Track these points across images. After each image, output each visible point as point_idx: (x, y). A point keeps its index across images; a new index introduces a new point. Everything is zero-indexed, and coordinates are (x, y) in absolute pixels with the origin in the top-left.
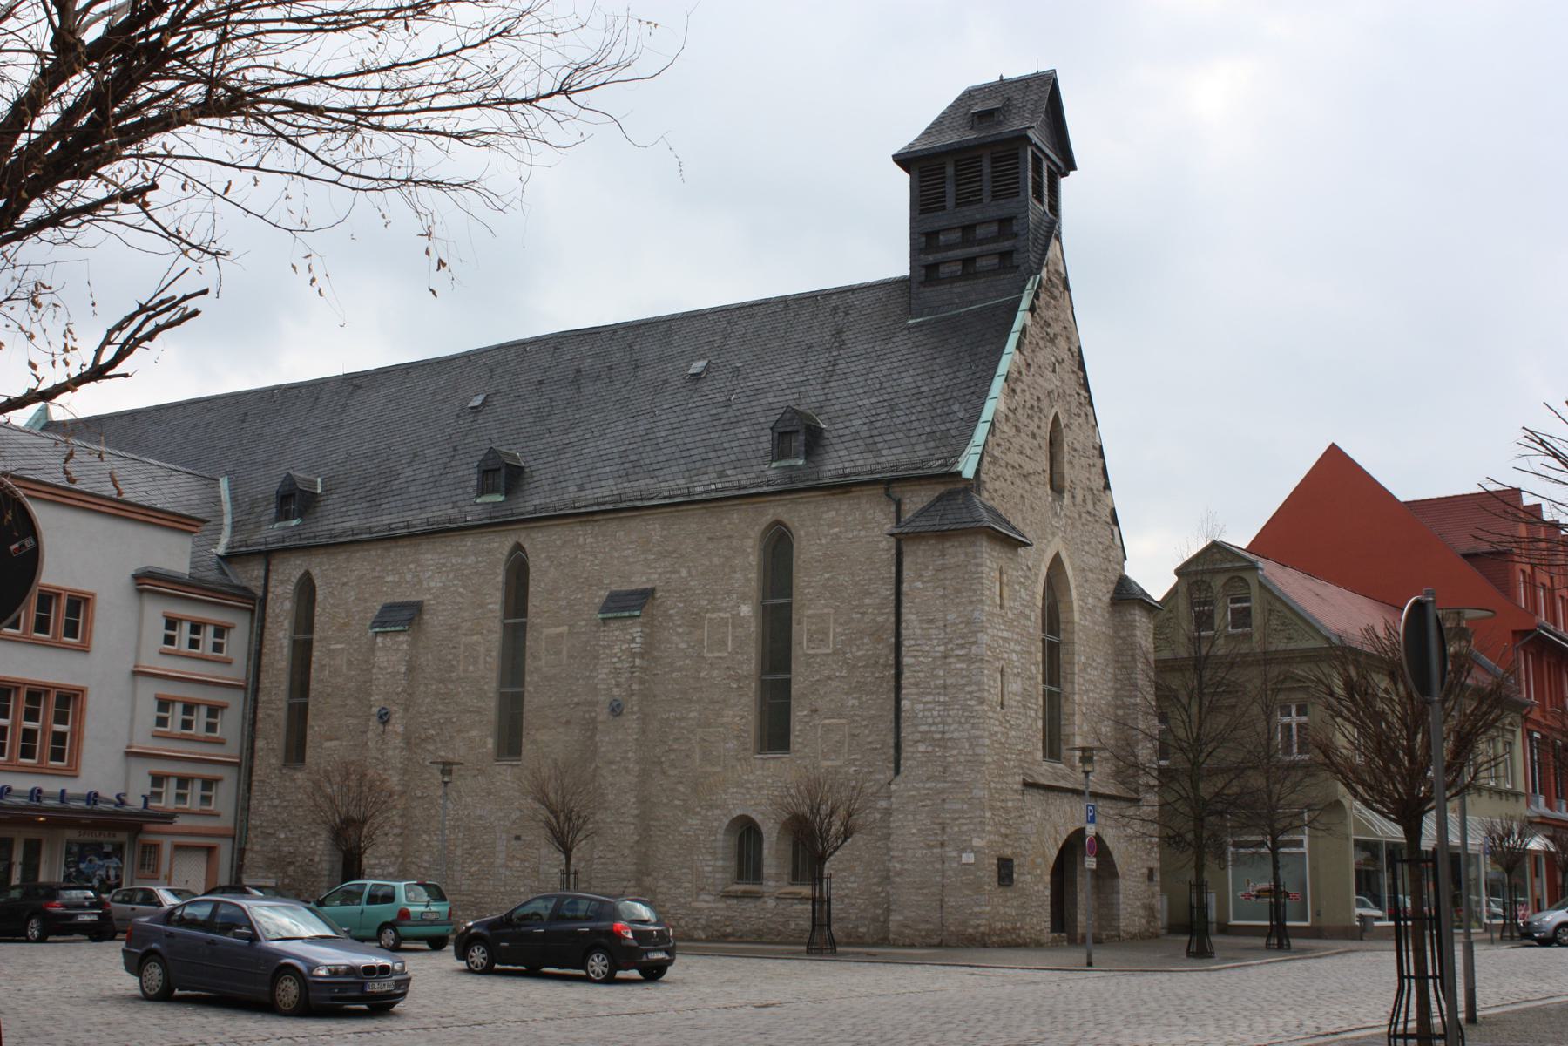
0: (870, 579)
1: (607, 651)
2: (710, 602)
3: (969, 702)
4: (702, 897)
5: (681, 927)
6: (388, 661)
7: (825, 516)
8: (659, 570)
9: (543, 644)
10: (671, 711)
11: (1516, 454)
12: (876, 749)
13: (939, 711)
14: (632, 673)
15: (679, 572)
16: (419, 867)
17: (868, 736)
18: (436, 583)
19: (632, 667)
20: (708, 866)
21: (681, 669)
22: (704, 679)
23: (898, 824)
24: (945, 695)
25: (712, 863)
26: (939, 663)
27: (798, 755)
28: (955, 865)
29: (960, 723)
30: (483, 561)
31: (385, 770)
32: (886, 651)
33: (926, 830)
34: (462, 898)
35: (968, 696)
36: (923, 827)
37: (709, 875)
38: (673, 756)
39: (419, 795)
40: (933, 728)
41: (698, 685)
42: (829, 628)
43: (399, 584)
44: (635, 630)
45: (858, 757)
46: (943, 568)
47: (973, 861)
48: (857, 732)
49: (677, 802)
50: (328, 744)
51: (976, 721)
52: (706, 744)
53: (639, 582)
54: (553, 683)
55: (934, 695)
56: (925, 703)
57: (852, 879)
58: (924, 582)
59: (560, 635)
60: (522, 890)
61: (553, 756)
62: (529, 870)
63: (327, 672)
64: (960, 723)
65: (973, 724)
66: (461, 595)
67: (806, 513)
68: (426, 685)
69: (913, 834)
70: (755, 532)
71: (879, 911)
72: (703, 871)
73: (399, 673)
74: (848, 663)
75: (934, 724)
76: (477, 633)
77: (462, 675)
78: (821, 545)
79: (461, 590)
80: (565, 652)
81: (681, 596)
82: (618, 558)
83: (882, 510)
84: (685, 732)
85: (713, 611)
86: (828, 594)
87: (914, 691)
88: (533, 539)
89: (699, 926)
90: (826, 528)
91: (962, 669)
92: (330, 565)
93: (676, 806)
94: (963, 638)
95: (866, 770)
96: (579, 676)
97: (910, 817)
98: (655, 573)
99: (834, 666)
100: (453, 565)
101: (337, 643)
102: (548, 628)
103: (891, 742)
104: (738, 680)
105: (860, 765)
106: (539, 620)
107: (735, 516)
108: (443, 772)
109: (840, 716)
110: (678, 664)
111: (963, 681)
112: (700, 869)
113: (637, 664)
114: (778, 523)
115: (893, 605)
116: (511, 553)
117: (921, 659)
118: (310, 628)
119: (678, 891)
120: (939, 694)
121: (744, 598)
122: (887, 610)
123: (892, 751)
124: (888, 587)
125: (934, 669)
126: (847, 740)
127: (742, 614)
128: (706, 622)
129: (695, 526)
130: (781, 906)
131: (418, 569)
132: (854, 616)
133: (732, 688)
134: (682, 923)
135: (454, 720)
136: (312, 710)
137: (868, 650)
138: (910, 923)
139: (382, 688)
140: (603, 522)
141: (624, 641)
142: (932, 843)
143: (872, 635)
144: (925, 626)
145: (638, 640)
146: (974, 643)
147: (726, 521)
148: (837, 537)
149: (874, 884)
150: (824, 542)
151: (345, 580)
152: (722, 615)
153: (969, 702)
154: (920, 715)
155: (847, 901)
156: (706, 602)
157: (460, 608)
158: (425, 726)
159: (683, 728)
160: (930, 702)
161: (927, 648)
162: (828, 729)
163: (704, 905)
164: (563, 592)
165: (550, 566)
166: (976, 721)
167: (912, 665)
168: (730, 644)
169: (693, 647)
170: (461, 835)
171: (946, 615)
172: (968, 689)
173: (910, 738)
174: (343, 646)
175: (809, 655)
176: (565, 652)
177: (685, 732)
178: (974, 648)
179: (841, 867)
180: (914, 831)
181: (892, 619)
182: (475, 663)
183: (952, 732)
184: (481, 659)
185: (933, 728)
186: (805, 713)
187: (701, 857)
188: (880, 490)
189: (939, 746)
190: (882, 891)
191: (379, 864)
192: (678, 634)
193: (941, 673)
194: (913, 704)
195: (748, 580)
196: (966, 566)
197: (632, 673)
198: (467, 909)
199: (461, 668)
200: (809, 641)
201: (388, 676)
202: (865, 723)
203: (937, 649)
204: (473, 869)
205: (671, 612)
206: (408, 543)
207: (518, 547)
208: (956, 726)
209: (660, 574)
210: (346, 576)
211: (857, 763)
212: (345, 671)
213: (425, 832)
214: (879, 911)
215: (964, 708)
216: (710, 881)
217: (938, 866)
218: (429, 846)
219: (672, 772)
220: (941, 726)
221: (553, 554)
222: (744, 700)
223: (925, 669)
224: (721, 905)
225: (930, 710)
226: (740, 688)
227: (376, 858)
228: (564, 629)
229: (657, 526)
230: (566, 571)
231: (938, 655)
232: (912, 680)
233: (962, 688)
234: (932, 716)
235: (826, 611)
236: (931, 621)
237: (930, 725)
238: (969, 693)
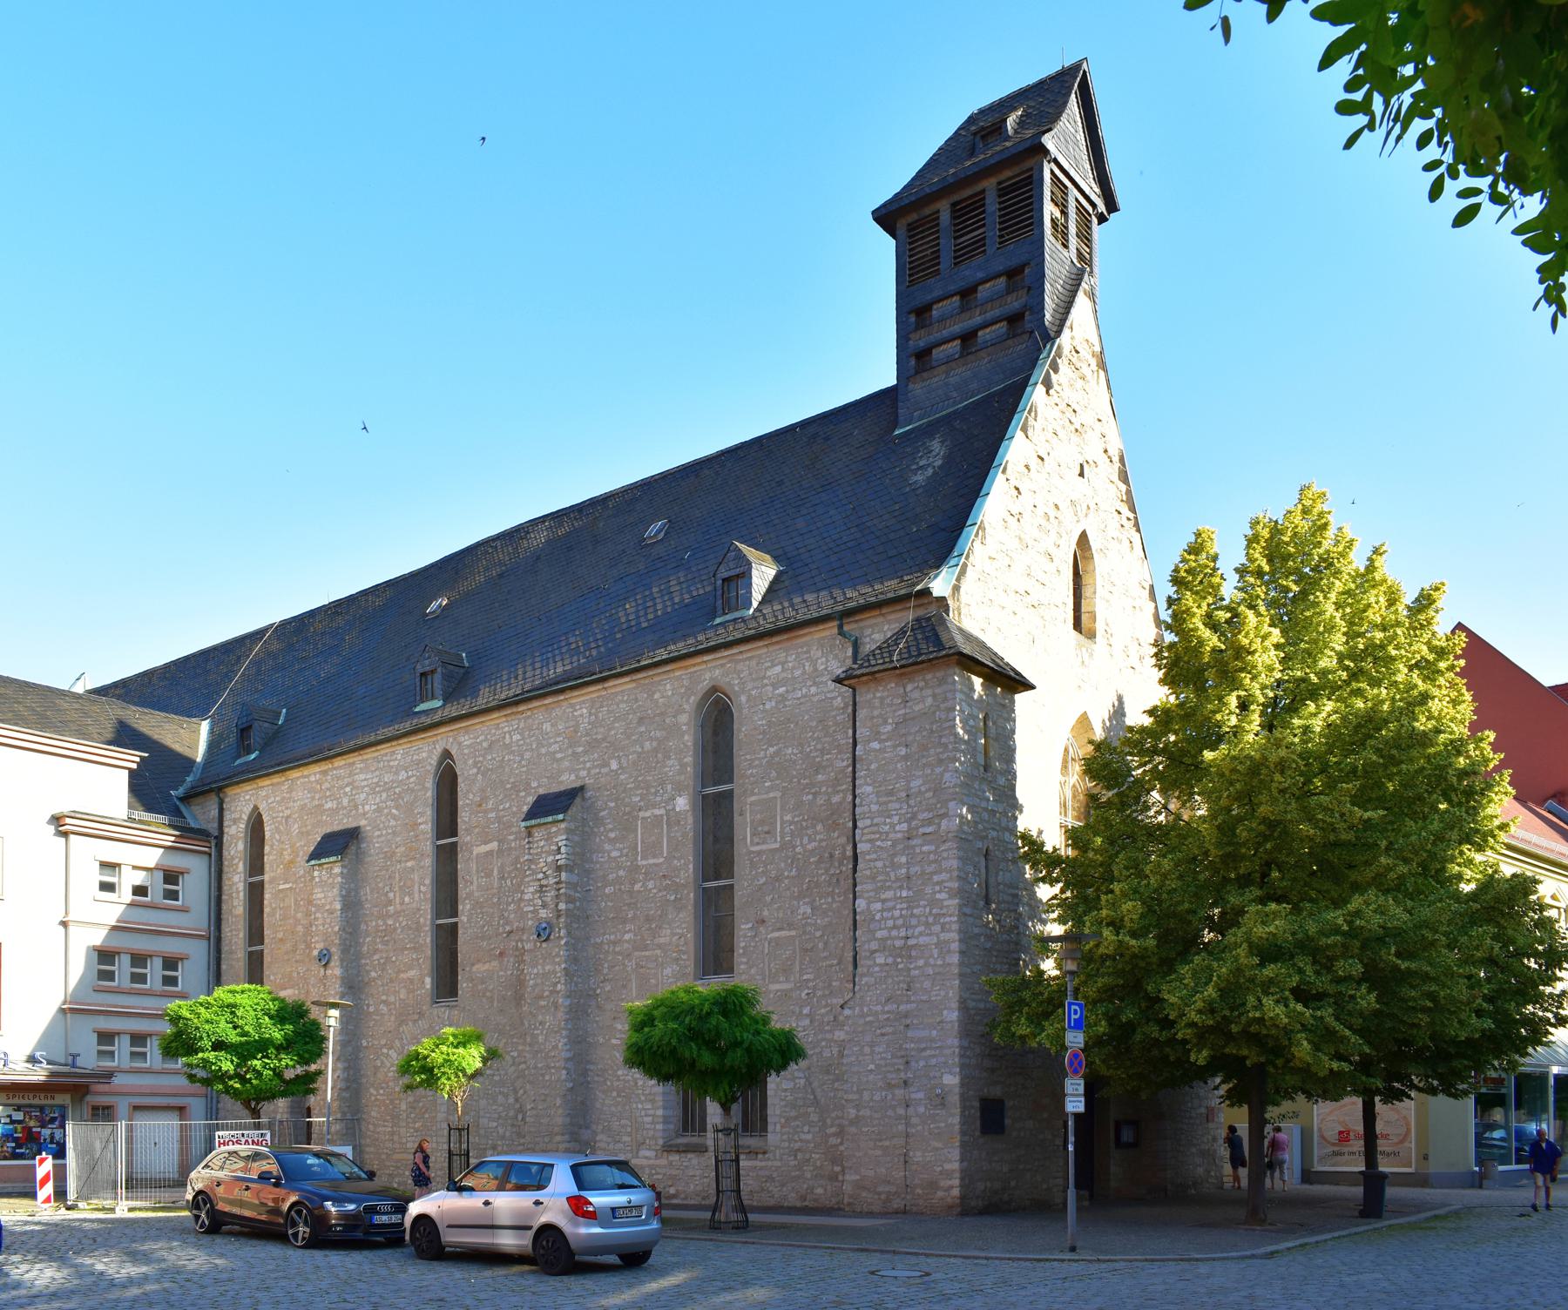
13: (902, 909)
25: (651, 1112)
64: (927, 924)
75: (895, 927)
97: (867, 1050)
117: (878, 843)
121: (679, 789)
141: (549, 853)
154: (878, 917)
162: (777, 943)
163: (645, 1162)
172: (936, 878)
175: (753, 852)
185: (894, 933)
200: (753, 835)
209: (589, 769)
216: (651, 1133)
225: (889, 910)
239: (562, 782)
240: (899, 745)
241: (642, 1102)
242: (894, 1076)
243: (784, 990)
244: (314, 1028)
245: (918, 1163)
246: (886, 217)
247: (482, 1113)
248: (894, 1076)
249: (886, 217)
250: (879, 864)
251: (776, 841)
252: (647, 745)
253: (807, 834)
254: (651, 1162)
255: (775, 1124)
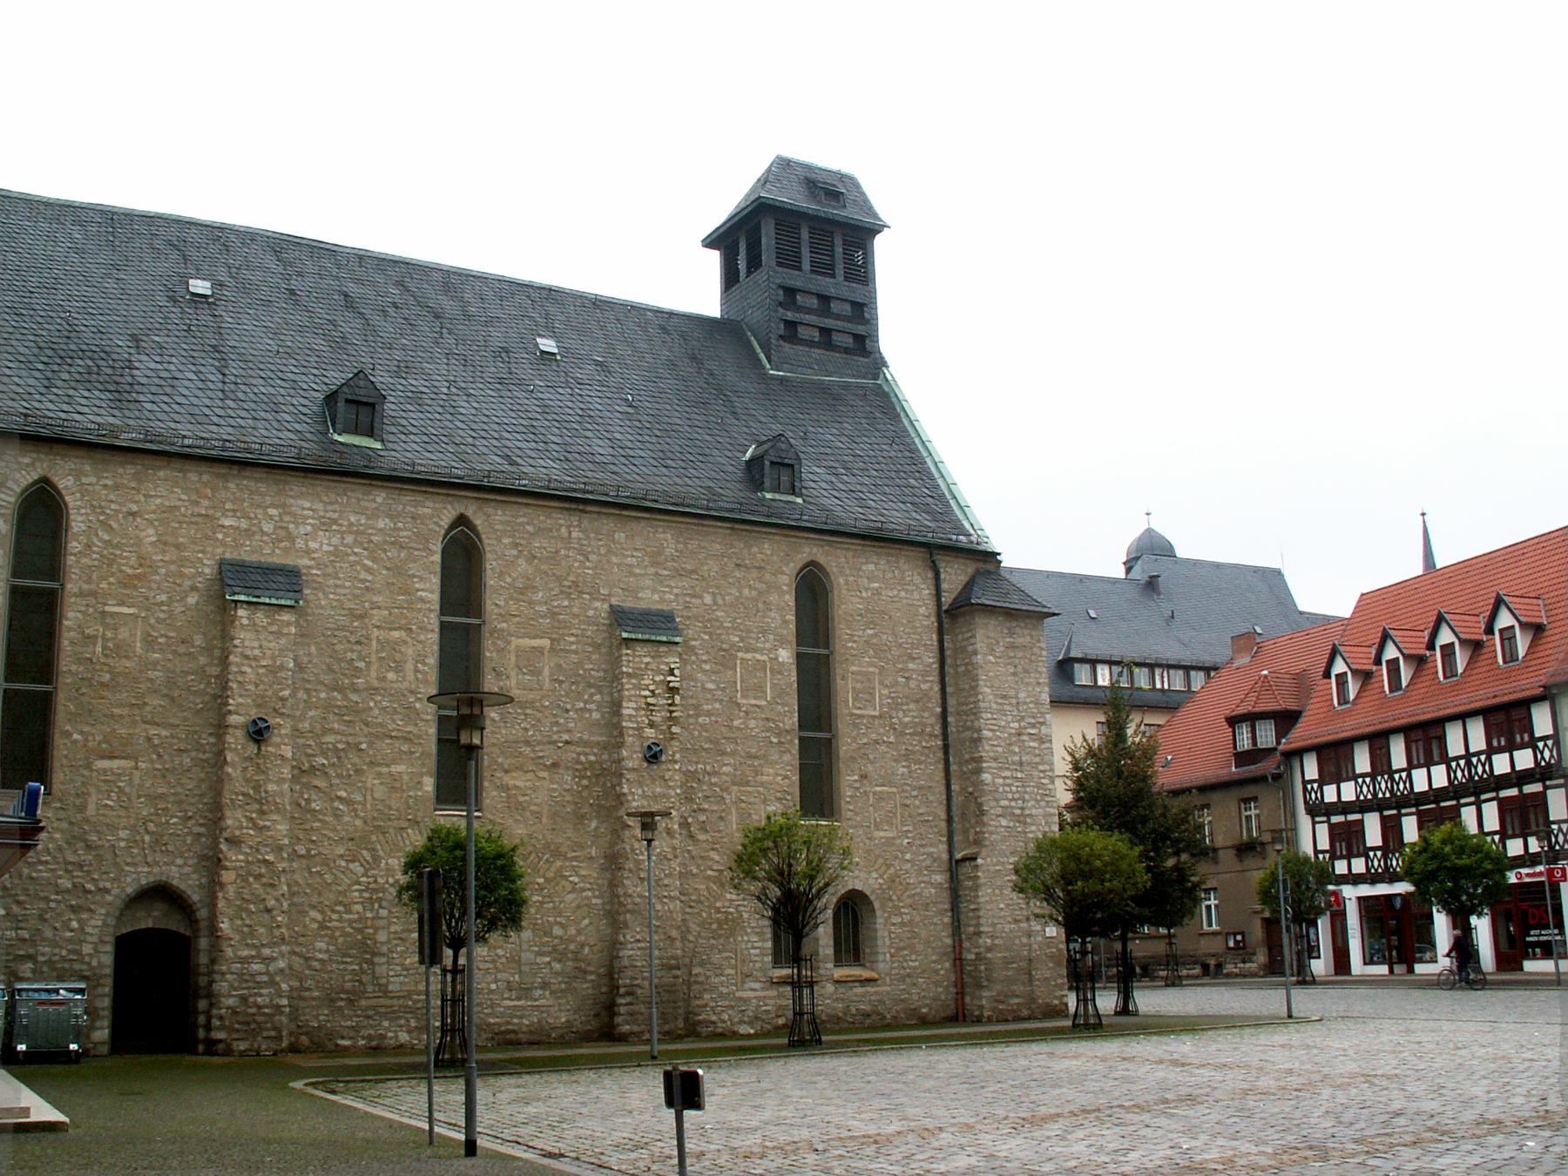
0: (912, 643)
1: (634, 681)
2: (742, 640)
3: (1043, 781)
4: (746, 986)
5: (724, 1022)
6: (261, 647)
7: (864, 568)
8: (675, 591)
9: (513, 658)
10: (697, 763)
11: (1060, 617)
12: (928, 821)
13: (1017, 787)
14: (671, 712)
15: (701, 597)
16: (307, 959)
17: (919, 807)
18: (323, 544)
19: (670, 705)
20: (754, 948)
21: (709, 714)
22: (738, 728)
23: (987, 899)
24: (1022, 771)
25: (759, 945)
26: (1014, 739)
27: (850, 823)
28: (1040, 939)
29: (1037, 800)
30: (405, 529)
31: (262, 813)
32: (932, 720)
33: (1013, 905)
34: (388, 1002)
35: (1042, 775)
36: (1010, 902)
37: (756, 959)
38: (703, 818)
39: (303, 852)
40: (1013, 804)
41: (732, 735)
42: (874, 688)
43: (248, 533)
44: (672, 660)
45: (911, 828)
46: (1012, 647)
47: (1055, 934)
48: (908, 802)
49: (710, 873)
50: (102, 764)
51: (1050, 799)
52: (743, 805)
53: (649, 599)
54: (528, 711)
55: (1012, 770)
56: (1004, 778)
57: (913, 957)
58: (995, 657)
59: (540, 650)
60: (493, 986)
61: (533, 808)
62: (504, 960)
63: (99, 649)
64: (1037, 800)
65: (1048, 802)
66: (369, 570)
67: (843, 560)
68: (308, 691)
69: (1002, 909)
70: (791, 569)
71: (940, 989)
72: (750, 954)
73: (282, 667)
74: (895, 729)
75: (1013, 799)
76: (400, 628)
77: (376, 683)
78: (861, 598)
79: (369, 563)
80: (546, 672)
81: (706, 627)
82: (619, 565)
83: (919, 574)
84: (718, 789)
85: (747, 651)
86: (872, 652)
87: (994, 765)
88: (489, 516)
89: (746, 1019)
90: (866, 581)
91: (1035, 748)
92: (99, 478)
93: (709, 878)
94: (1033, 717)
95: (919, 842)
96: (569, 707)
97: (997, 892)
98: (670, 593)
99: (882, 730)
100: (351, 524)
101: (122, 604)
102: (518, 637)
103: (943, 815)
104: (778, 735)
105: (914, 838)
106: (504, 625)
107: (766, 546)
108: (645, 827)
109: (891, 784)
110: (705, 707)
111: (1037, 760)
112: (745, 952)
113: (676, 702)
114: (813, 563)
115: (936, 673)
116: (453, 526)
117: (998, 733)
118: (53, 567)
119: (717, 980)
120: (1016, 770)
121: (782, 642)
122: (931, 679)
123: (943, 825)
124: (931, 655)
125: (1010, 745)
126: (899, 810)
127: (781, 660)
128: (738, 662)
129: (718, 547)
130: (841, 990)
131: (287, 518)
132: (900, 679)
133: (771, 742)
134: (726, 1017)
135: (364, 746)
136: (64, 704)
137: (914, 717)
138: (1002, 998)
139: (252, 687)
140: (595, 516)
141: (659, 672)
142: (1018, 918)
143: (918, 702)
144: (1000, 701)
145: (677, 672)
146: (1042, 724)
147: (755, 549)
148: (877, 592)
149: (935, 962)
150: (864, 594)
151: (135, 508)
152: (758, 656)
153: (1043, 781)
154: (1001, 789)
155: (908, 980)
156: (737, 639)
157: (367, 589)
158: (310, 751)
159: (715, 784)
160: (1008, 778)
161: (1003, 723)
162: (880, 797)
163: (751, 994)
164: (540, 594)
165: (517, 557)
166: (1050, 799)
167: (990, 739)
168: (768, 692)
169: (723, 690)
170: (383, 913)
171: (1017, 693)
172: (1041, 768)
173: (992, 812)
174: (131, 611)
175: (855, 715)
176: (546, 672)
177: (718, 789)
178: (1043, 728)
179: (902, 944)
180: (1002, 906)
181: (937, 688)
182: (398, 669)
183: (1030, 809)
184: (409, 666)
185: (1013, 804)
186: (856, 777)
187: (746, 938)
188: (920, 553)
189: (1019, 822)
190: (941, 969)
191: (259, 956)
192: (705, 671)
193: (1017, 750)
194: (994, 778)
195: (785, 622)
196: (1031, 648)
197: (671, 712)
198: (400, 1018)
199: (374, 674)
200: (854, 699)
201: (261, 671)
202: (915, 793)
203: (1012, 725)
204: (408, 961)
205: (693, 643)
206: (265, 476)
207: (462, 520)
208: (1033, 803)
209: (676, 595)
210: (137, 502)
211: (910, 835)
212: (139, 651)
213: (314, 907)
214: (940, 989)
215: (1040, 786)
216: (758, 965)
217: (1025, 940)
218: (322, 926)
219: (702, 837)
220: (1020, 802)
221: (522, 542)
222: (787, 757)
223: (1003, 744)
224: (773, 993)
225: (1009, 785)
226: (780, 743)
227: (254, 946)
228: (546, 642)
229: (669, 536)
230: (544, 567)
231: (1013, 731)
232: (992, 754)
233: (1035, 766)
234: (1011, 791)
235: (871, 669)
236: (1004, 697)
237: (1011, 800)
238: (1041, 771)
239: (641, 599)
240: (1008, 664)
241: (747, 934)
242: (1019, 913)
243: (888, 838)
244: (452, 838)
245: (1038, 980)
246: (711, 242)
247: (525, 947)
248: (1019, 913)
249: (711, 242)
250: (999, 749)
251: (875, 709)
252: (746, 592)
253: (902, 709)
254: (759, 994)
255: (885, 954)
